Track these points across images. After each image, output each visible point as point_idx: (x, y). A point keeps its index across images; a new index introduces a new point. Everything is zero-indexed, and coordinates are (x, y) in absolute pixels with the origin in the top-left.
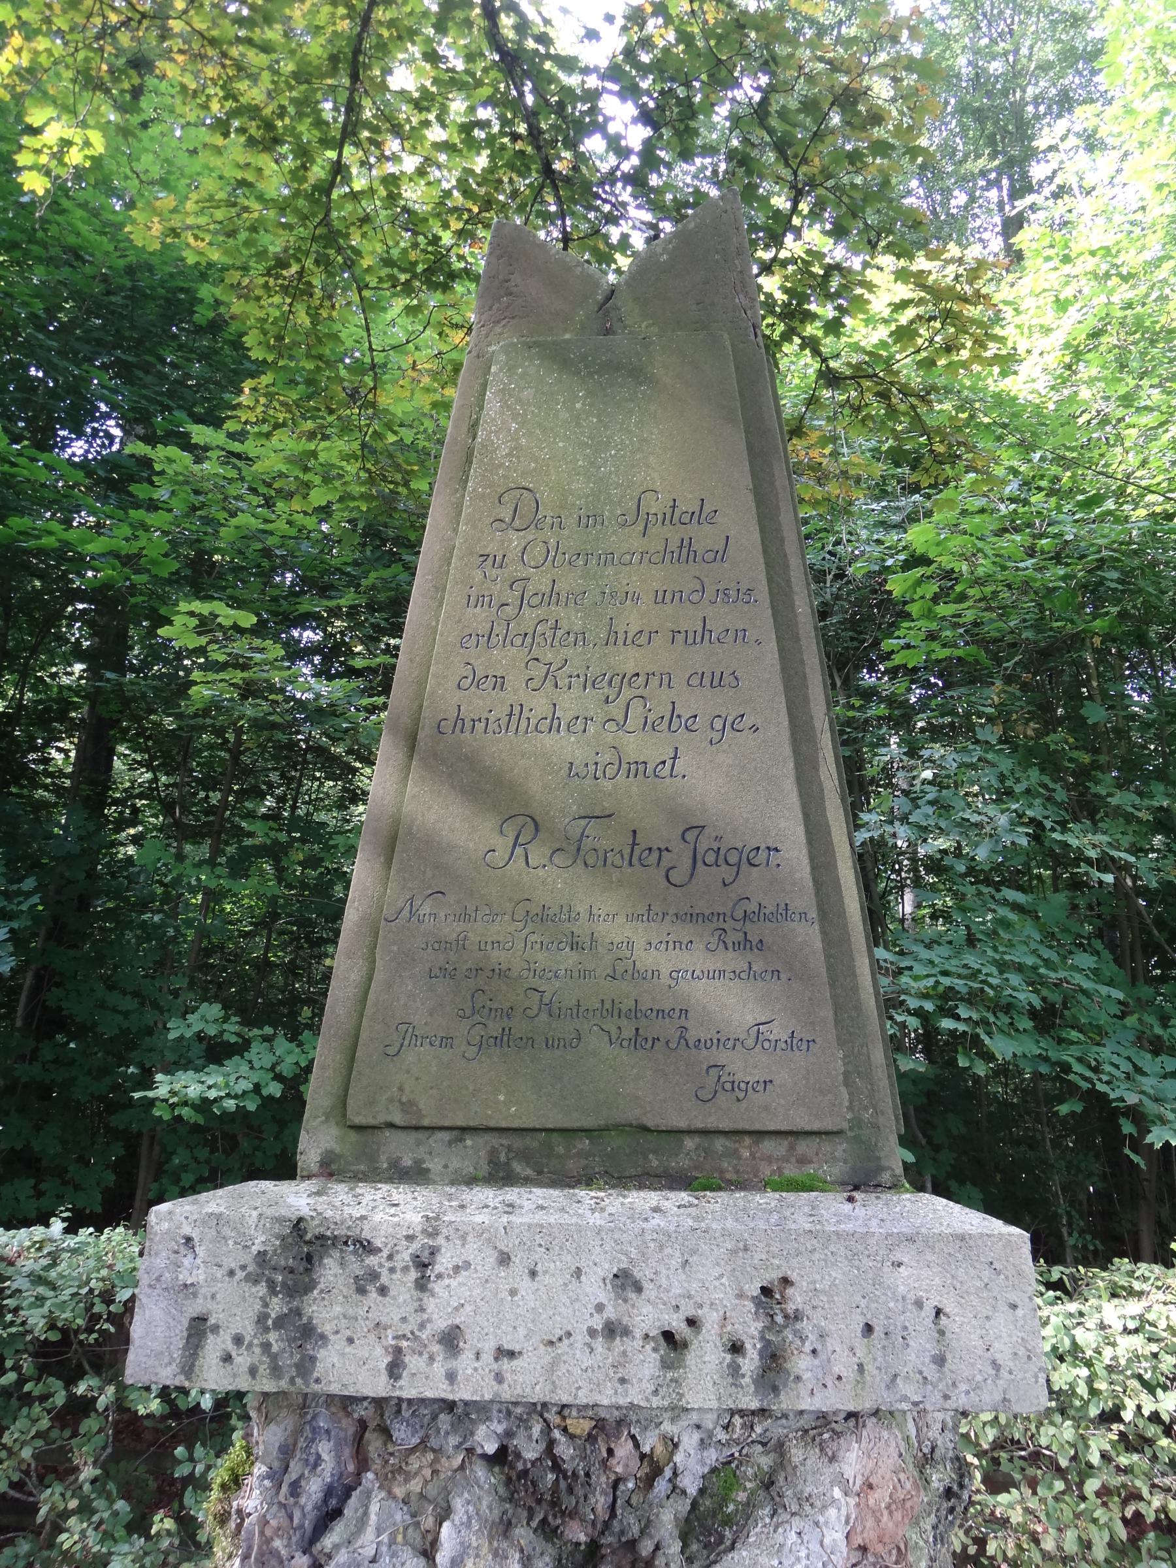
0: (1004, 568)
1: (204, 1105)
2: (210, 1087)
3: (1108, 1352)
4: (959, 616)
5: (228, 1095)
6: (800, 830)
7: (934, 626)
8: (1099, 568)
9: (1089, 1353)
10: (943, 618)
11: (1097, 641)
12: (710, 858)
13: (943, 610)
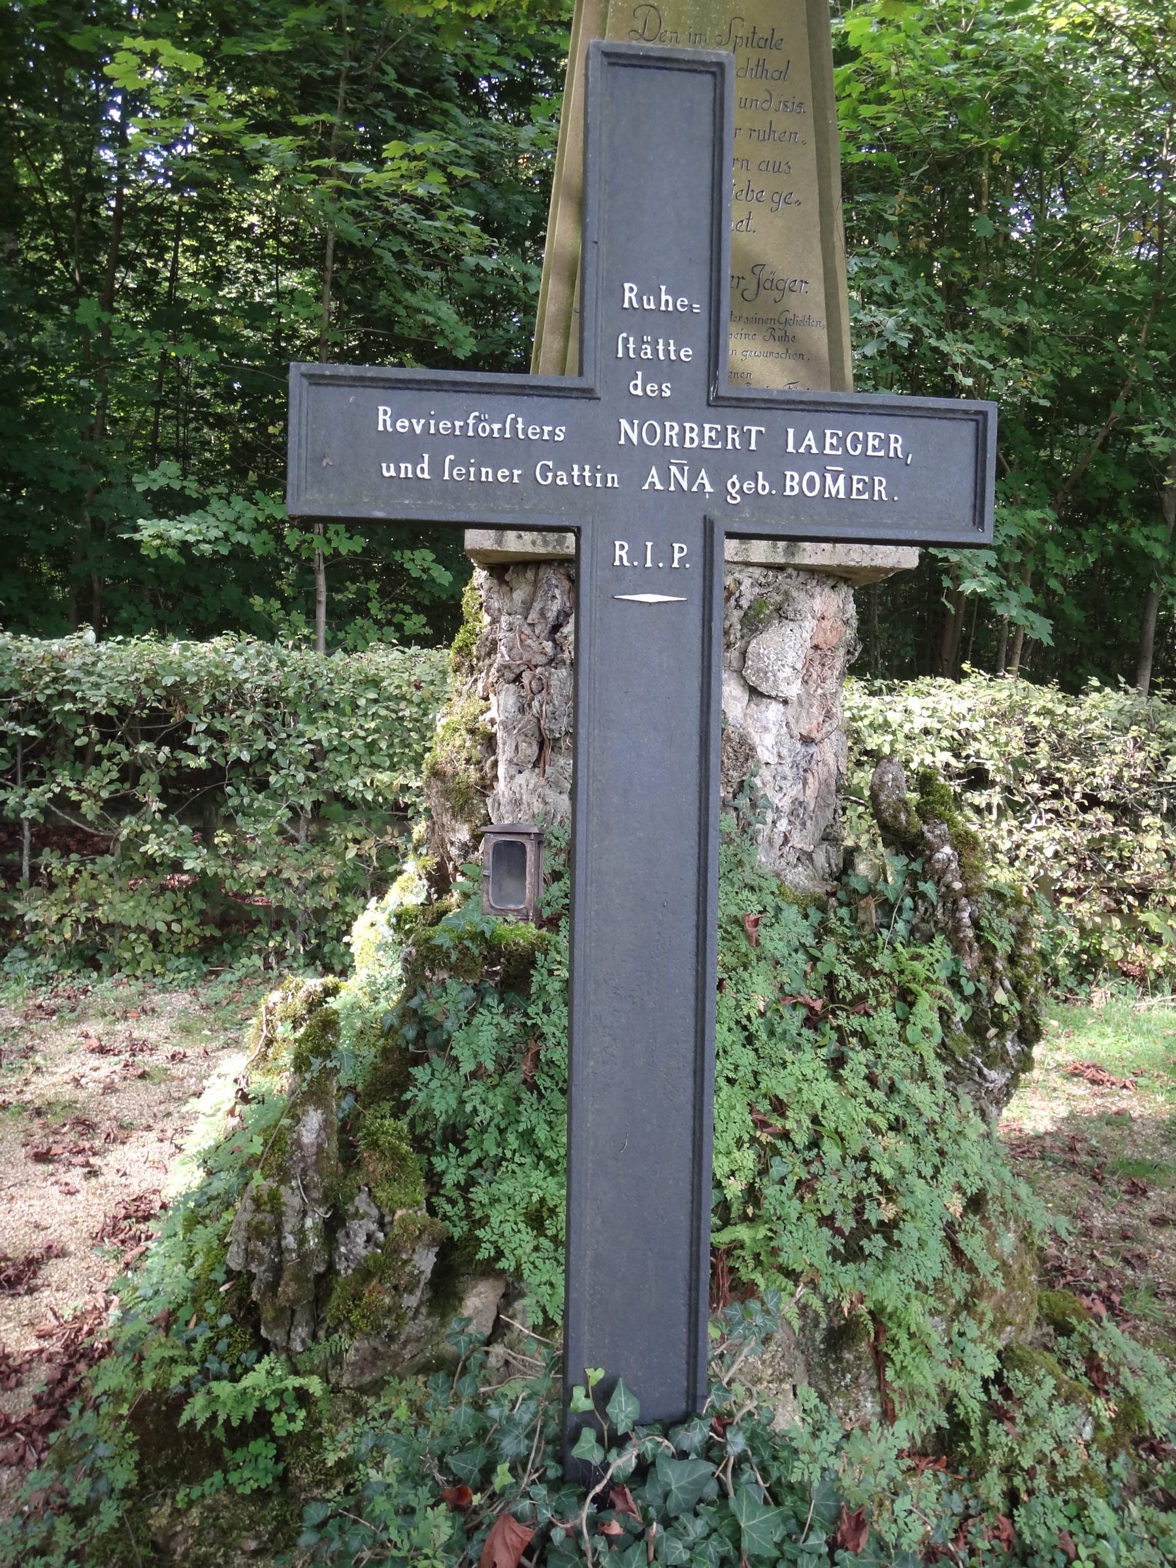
0: (929, 72)
1: (185, 547)
2: (187, 533)
3: (907, 726)
4: (878, 118)
5: (204, 541)
6: (821, 271)
7: (854, 127)
8: (1012, 80)
9: (894, 726)
10: (864, 120)
11: (997, 157)
12: (768, 285)
13: (867, 111)
